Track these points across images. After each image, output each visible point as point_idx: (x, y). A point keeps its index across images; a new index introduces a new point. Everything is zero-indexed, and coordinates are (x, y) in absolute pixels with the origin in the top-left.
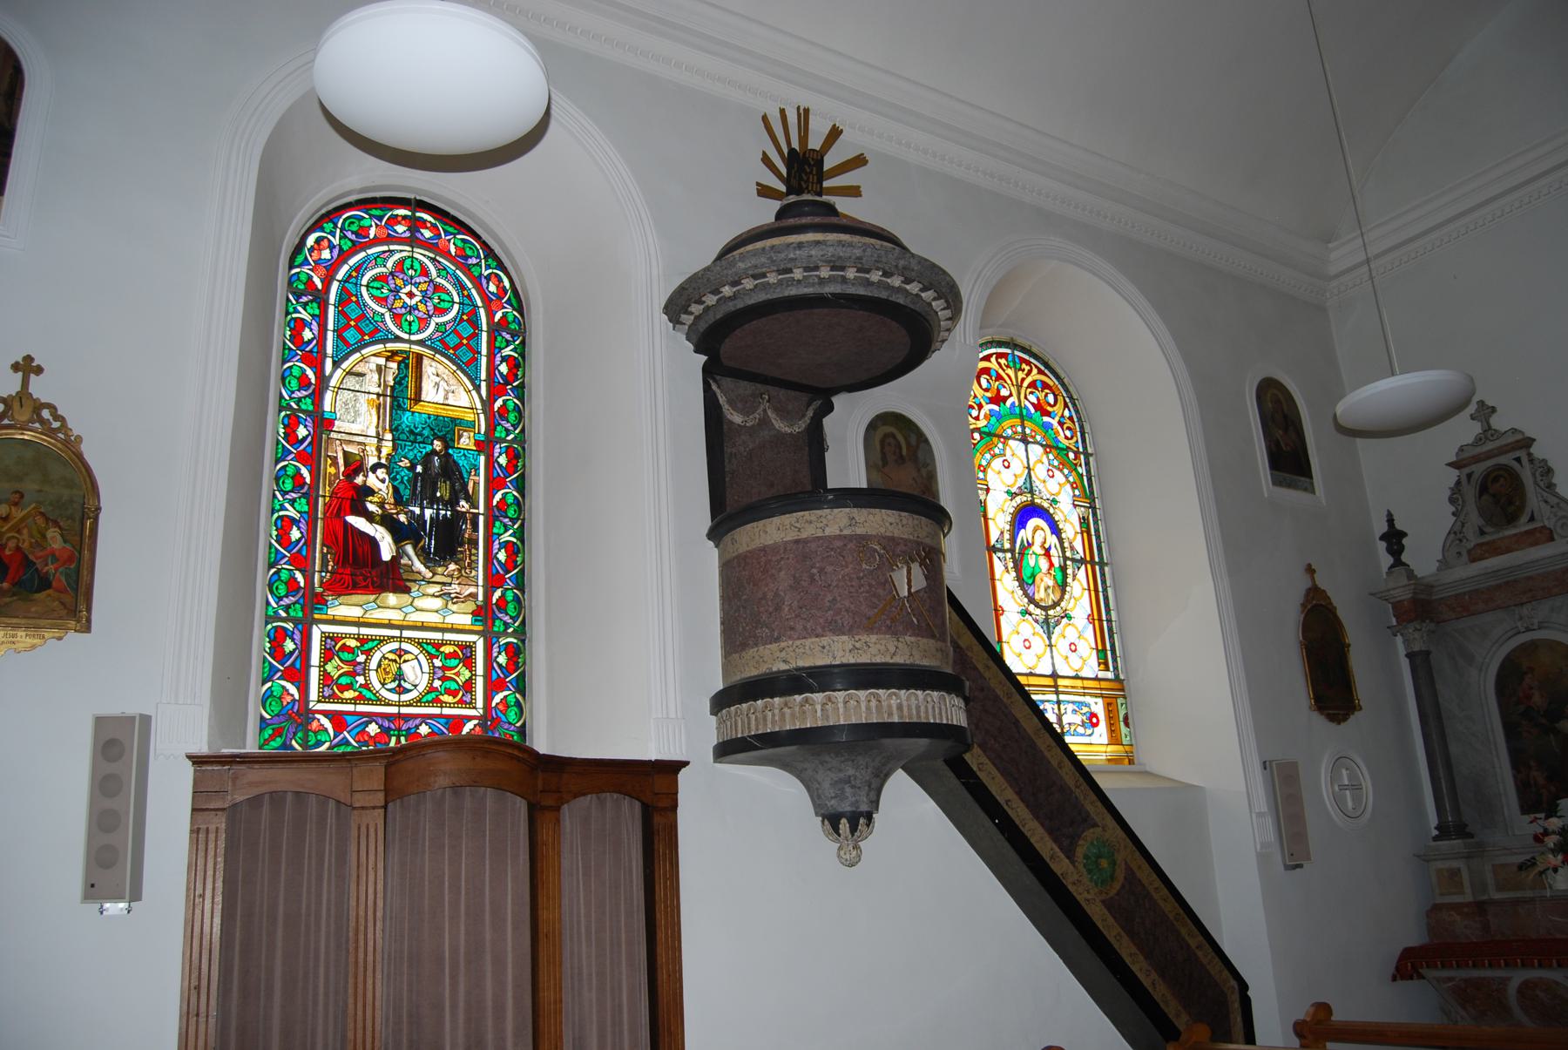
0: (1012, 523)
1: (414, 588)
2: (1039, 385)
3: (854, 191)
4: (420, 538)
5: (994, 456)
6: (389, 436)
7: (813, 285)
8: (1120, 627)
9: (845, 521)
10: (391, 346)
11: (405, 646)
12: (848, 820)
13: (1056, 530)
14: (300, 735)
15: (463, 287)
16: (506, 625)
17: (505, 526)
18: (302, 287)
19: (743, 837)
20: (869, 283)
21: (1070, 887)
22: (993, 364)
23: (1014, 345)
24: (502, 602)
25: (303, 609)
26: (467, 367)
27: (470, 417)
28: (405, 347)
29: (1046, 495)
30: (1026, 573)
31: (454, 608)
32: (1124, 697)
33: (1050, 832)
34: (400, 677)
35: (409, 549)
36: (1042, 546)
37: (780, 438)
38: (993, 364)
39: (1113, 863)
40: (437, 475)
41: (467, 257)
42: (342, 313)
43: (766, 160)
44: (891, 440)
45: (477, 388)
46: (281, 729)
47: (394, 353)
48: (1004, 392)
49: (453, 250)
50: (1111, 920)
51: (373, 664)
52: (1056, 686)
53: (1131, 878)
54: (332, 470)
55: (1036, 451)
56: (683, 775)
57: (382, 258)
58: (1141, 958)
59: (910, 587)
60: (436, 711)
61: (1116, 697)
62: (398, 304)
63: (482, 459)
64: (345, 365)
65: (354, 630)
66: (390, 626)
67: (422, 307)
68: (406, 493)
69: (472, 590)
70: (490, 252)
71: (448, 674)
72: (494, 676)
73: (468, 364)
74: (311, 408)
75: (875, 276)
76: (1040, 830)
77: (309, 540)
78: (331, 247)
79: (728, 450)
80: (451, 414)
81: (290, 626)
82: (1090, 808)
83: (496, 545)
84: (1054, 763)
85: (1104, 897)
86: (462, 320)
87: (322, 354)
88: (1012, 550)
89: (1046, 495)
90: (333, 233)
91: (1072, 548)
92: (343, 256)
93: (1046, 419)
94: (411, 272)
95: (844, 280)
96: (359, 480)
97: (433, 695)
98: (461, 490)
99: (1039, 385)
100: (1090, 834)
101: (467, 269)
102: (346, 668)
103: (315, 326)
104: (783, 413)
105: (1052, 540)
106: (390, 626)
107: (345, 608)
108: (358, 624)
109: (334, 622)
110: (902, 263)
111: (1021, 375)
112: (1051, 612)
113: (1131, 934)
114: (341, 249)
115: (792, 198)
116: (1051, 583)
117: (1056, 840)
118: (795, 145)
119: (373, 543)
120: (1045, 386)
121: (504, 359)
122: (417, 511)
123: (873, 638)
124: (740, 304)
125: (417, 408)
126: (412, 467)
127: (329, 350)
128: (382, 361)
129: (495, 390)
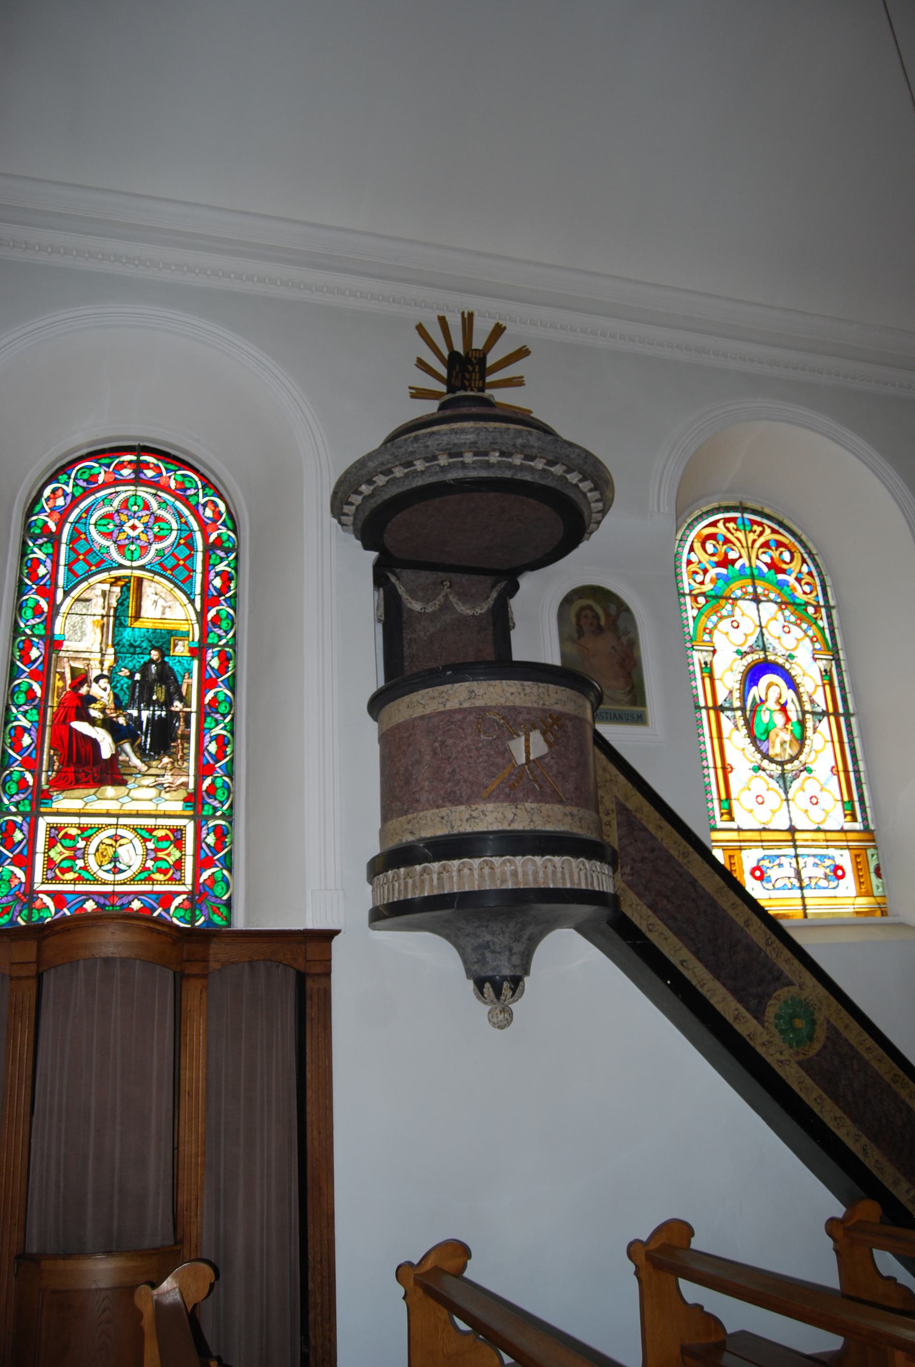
0: (743, 682)
1: (131, 780)
2: (772, 544)
3: (516, 382)
4: (138, 736)
5: (721, 618)
6: (111, 651)
7: (436, 473)
8: (869, 776)
9: (465, 695)
10: (115, 573)
11: (121, 832)
12: (499, 984)
13: (792, 684)
14: (25, 912)
15: (181, 516)
16: (215, 809)
17: (216, 721)
18: (38, 531)
19: (394, 999)
20: (489, 465)
21: (760, 1050)
22: (721, 529)
23: (743, 509)
24: (212, 790)
25: (31, 804)
26: (183, 584)
27: (184, 628)
28: (127, 572)
29: (781, 651)
30: (758, 731)
31: (167, 796)
32: (875, 847)
33: (734, 992)
34: (115, 859)
35: (127, 747)
36: (778, 702)
37: (463, 621)
38: (721, 529)
39: (813, 1022)
40: (155, 680)
41: (186, 489)
42: (73, 549)
43: (421, 364)
44: (588, 612)
45: (192, 602)
46: (10, 907)
47: (118, 579)
48: (732, 555)
49: (173, 485)
50: (809, 1082)
51: (92, 849)
52: (794, 840)
53: (834, 1036)
54: (60, 684)
55: (768, 609)
56: (336, 942)
57: (108, 499)
58: (848, 1121)
59: (528, 753)
60: (148, 888)
61: (865, 848)
62: (122, 536)
63: (195, 663)
64: (75, 594)
65: (75, 820)
66: (108, 815)
67: (143, 537)
68: (125, 699)
69: (184, 779)
70: (207, 483)
71: (160, 855)
72: (203, 855)
73: (183, 582)
74: (43, 632)
75: (494, 457)
76: (723, 991)
77: (39, 747)
78: (65, 495)
79: (407, 636)
80: (168, 627)
81: (19, 819)
82: (783, 966)
83: (207, 739)
84: (740, 922)
85: (801, 1057)
86: (179, 544)
87: (55, 585)
88: (743, 709)
89: (781, 651)
90: (67, 484)
91: (812, 702)
92: (75, 501)
93: (781, 577)
94: (135, 508)
95: (464, 465)
96: (83, 690)
97: (146, 874)
98: (175, 692)
99: (772, 544)
100: (784, 993)
101: (185, 501)
102: (67, 853)
103: (49, 563)
104: (464, 596)
105: (789, 695)
106: (108, 815)
107: (64, 802)
108: (79, 815)
109: (58, 814)
110: (519, 441)
111: (751, 537)
112: (788, 767)
113: (836, 1098)
114: (73, 495)
115: (451, 396)
116: (787, 737)
117: (740, 1000)
118: (459, 347)
119: (94, 744)
120: (779, 544)
121: (217, 574)
122: (135, 713)
123: (490, 806)
124: (379, 500)
125: (137, 624)
126: (131, 676)
127: (61, 581)
128: (106, 587)
129: (209, 601)
